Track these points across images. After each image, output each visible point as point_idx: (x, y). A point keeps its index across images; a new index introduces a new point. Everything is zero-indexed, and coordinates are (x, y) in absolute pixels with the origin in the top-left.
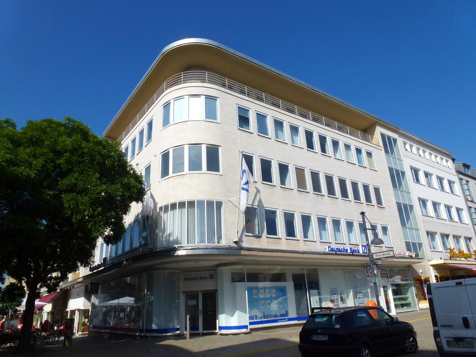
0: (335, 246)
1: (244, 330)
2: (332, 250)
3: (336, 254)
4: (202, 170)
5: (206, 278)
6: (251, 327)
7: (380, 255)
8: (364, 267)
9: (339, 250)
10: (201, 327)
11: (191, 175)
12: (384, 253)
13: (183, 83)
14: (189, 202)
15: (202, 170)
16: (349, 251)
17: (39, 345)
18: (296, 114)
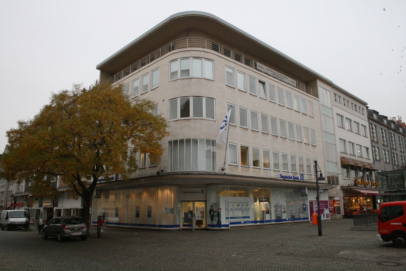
0: (284, 174)
1: (226, 228)
2: (282, 177)
3: (284, 180)
4: (189, 117)
5: (199, 192)
6: (230, 226)
7: (324, 188)
8: (299, 189)
9: (286, 177)
10: (192, 140)
11: (194, 120)
12: (326, 187)
13: (172, 50)
14: (174, 141)
15: (189, 117)
16: (292, 178)
17: (103, 232)
18: (242, 63)
